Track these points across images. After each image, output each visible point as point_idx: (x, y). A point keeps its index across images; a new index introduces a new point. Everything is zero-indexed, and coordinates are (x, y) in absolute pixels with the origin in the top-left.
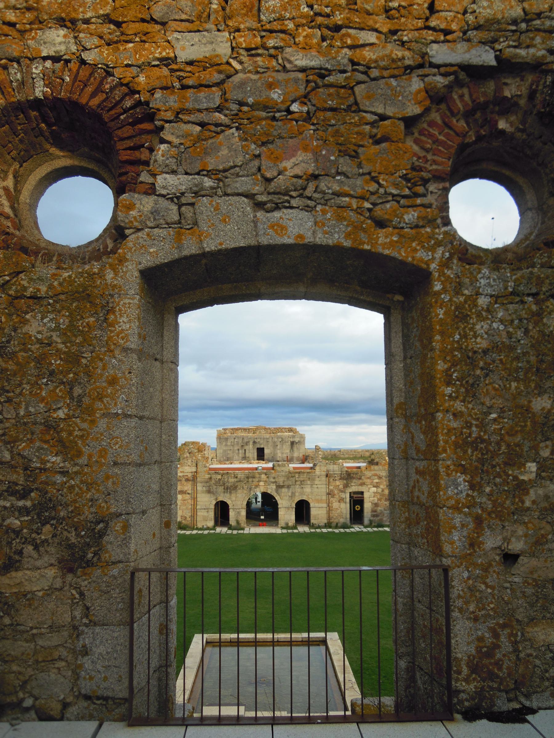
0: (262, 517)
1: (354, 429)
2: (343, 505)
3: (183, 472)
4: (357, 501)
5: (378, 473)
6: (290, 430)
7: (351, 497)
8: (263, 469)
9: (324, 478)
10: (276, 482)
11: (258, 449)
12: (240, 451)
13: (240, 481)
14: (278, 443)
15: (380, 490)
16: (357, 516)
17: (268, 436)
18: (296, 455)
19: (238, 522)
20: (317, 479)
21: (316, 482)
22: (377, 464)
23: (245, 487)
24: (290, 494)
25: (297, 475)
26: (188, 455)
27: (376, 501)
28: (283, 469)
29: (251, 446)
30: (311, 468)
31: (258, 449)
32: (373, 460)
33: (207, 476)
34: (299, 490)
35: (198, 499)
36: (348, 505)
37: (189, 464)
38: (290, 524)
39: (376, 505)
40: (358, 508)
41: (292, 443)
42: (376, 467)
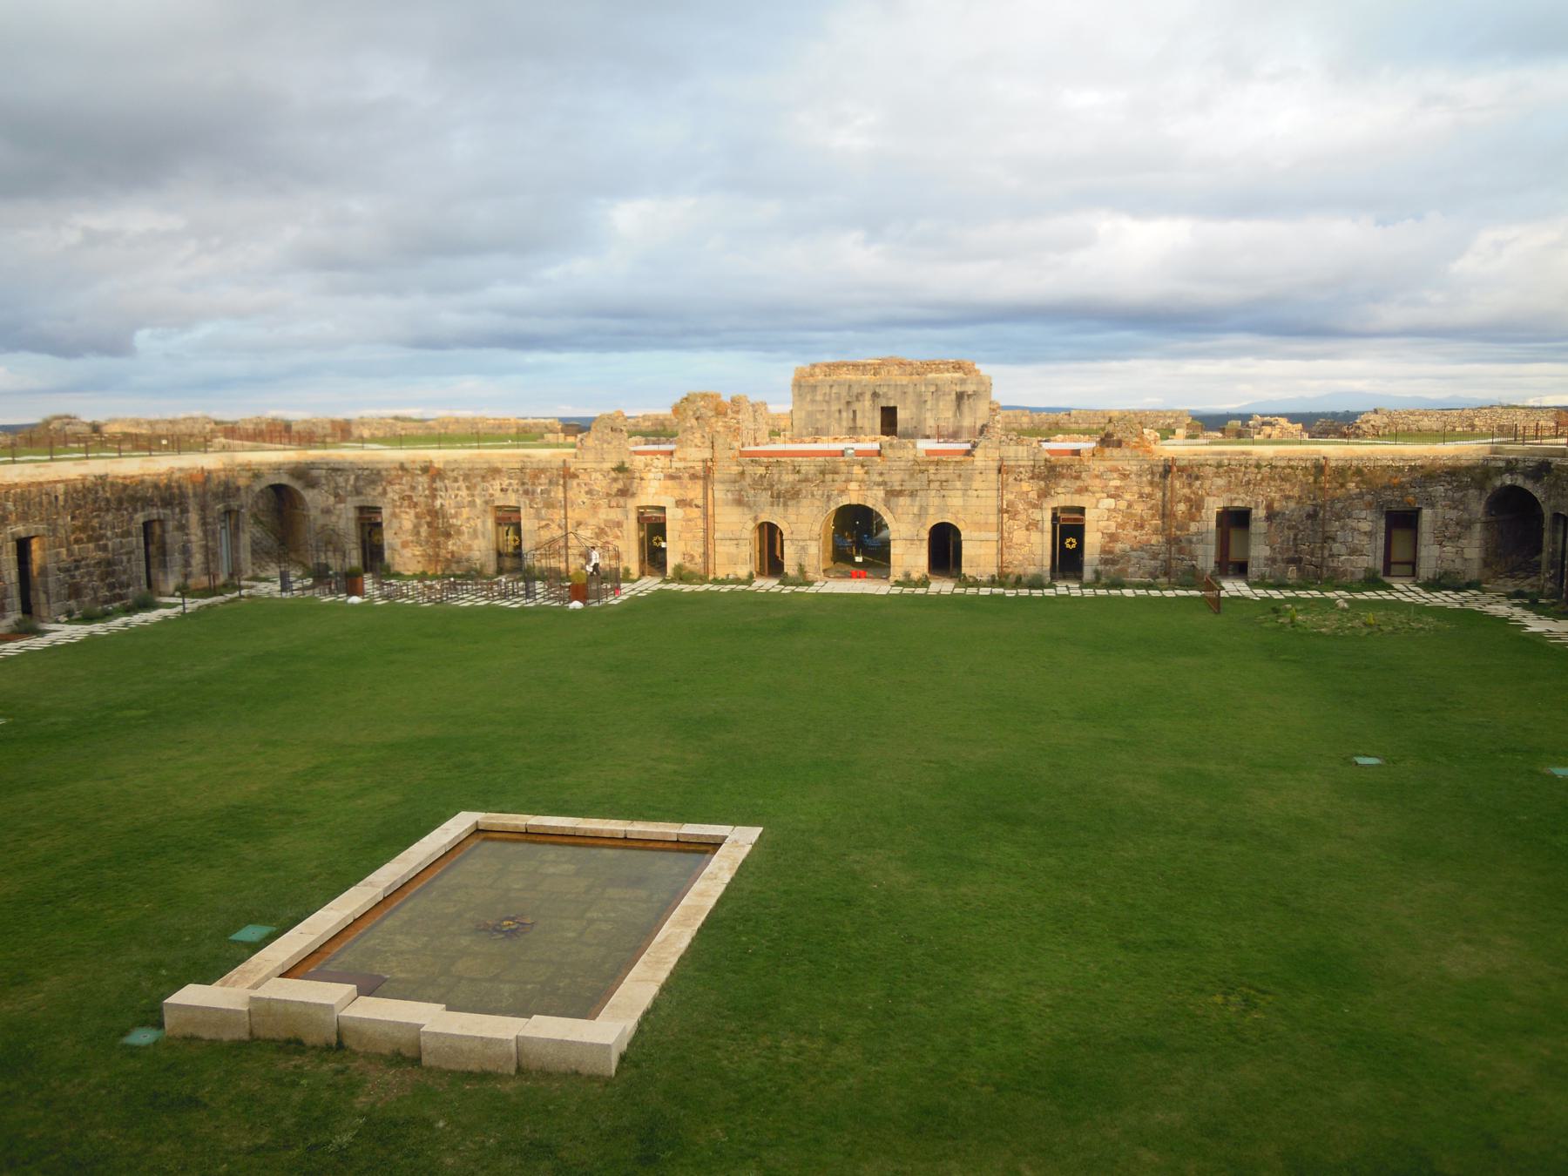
0: (859, 559)
1: (1224, 366)
2: (1035, 536)
3: (685, 460)
4: (1069, 528)
5: (1120, 464)
6: (958, 367)
7: (1055, 518)
8: (858, 453)
9: (993, 476)
10: (884, 483)
11: (883, 409)
12: (844, 414)
13: (806, 480)
14: (929, 397)
15: (1122, 505)
16: (1067, 561)
17: (905, 380)
18: (967, 422)
19: (801, 568)
20: (978, 477)
21: (975, 485)
22: (1119, 444)
23: (818, 493)
24: (916, 510)
25: (932, 469)
26: (694, 422)
27: (1113, 529)
28: (900, 453)
29: (867, 403)
30: (968, 453)
31: (883, 409)
32: (1109, 435)
33: (735, 469)
34: (937, 501)
35: (718, 519)
36: (1048, 537)
37: (698, 441)
38: (915, 576)
39: (1113, 538)
40: (1071, 543)
41: (960, 397)
42: (1116, 452)
